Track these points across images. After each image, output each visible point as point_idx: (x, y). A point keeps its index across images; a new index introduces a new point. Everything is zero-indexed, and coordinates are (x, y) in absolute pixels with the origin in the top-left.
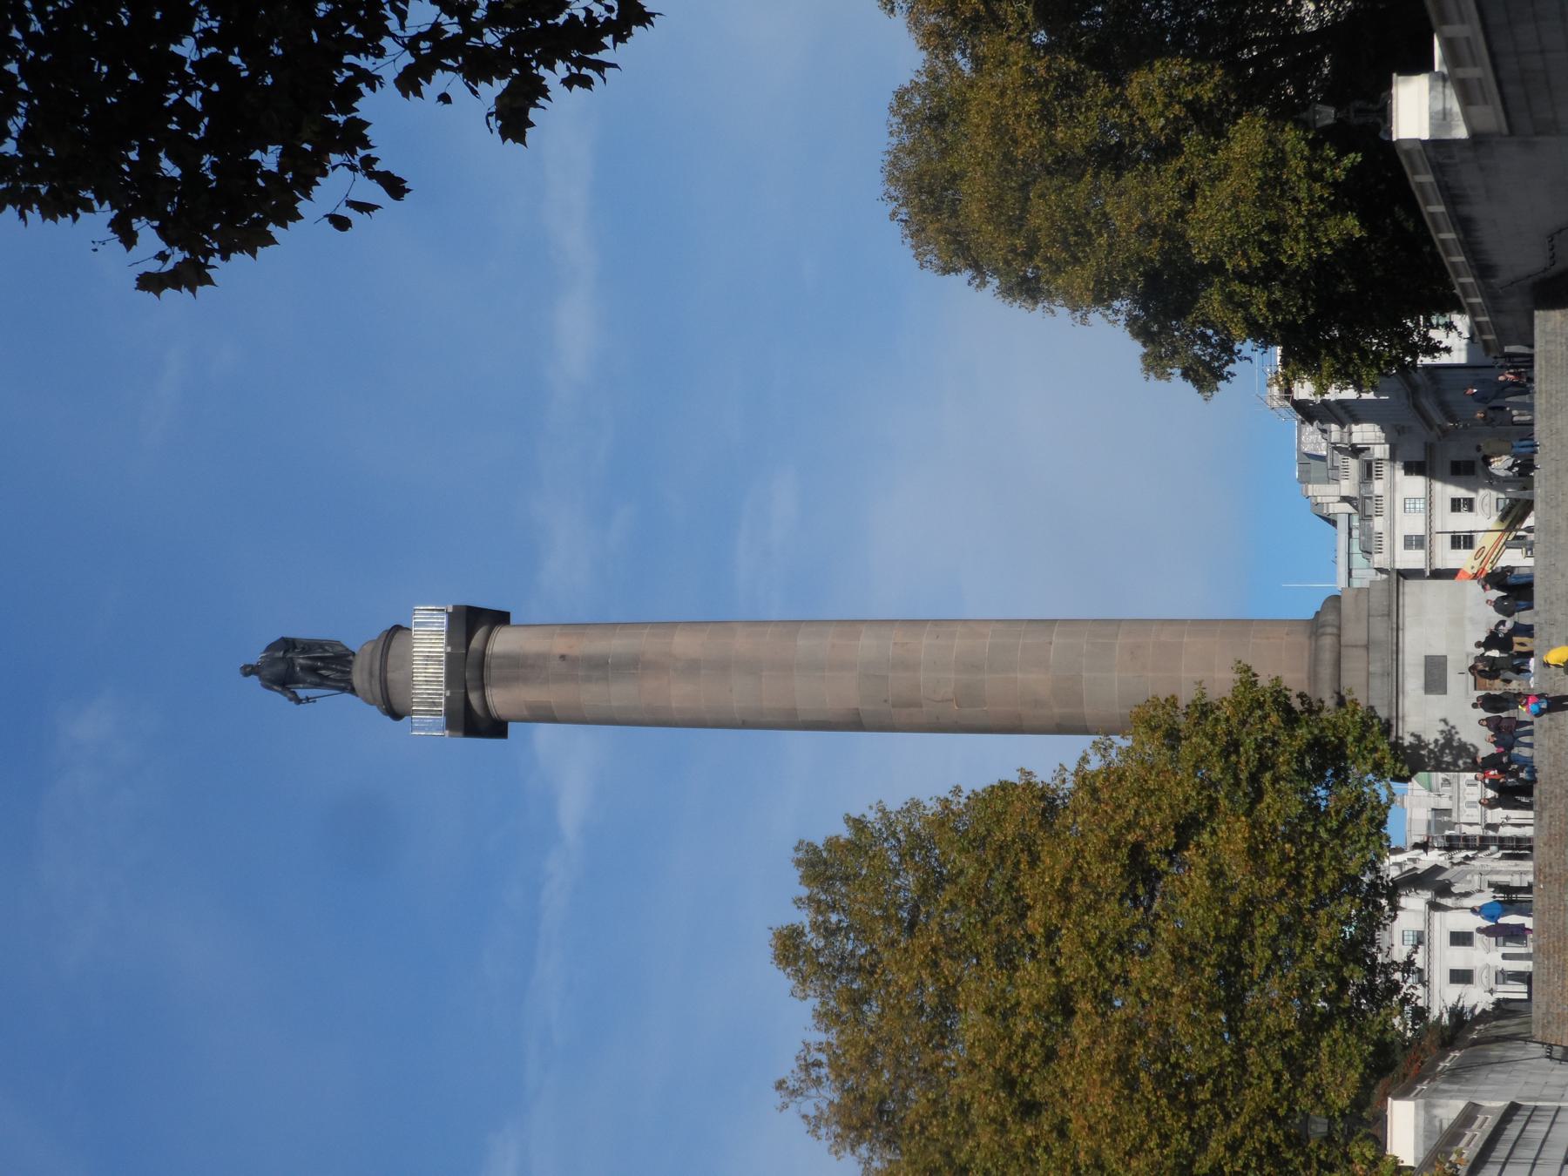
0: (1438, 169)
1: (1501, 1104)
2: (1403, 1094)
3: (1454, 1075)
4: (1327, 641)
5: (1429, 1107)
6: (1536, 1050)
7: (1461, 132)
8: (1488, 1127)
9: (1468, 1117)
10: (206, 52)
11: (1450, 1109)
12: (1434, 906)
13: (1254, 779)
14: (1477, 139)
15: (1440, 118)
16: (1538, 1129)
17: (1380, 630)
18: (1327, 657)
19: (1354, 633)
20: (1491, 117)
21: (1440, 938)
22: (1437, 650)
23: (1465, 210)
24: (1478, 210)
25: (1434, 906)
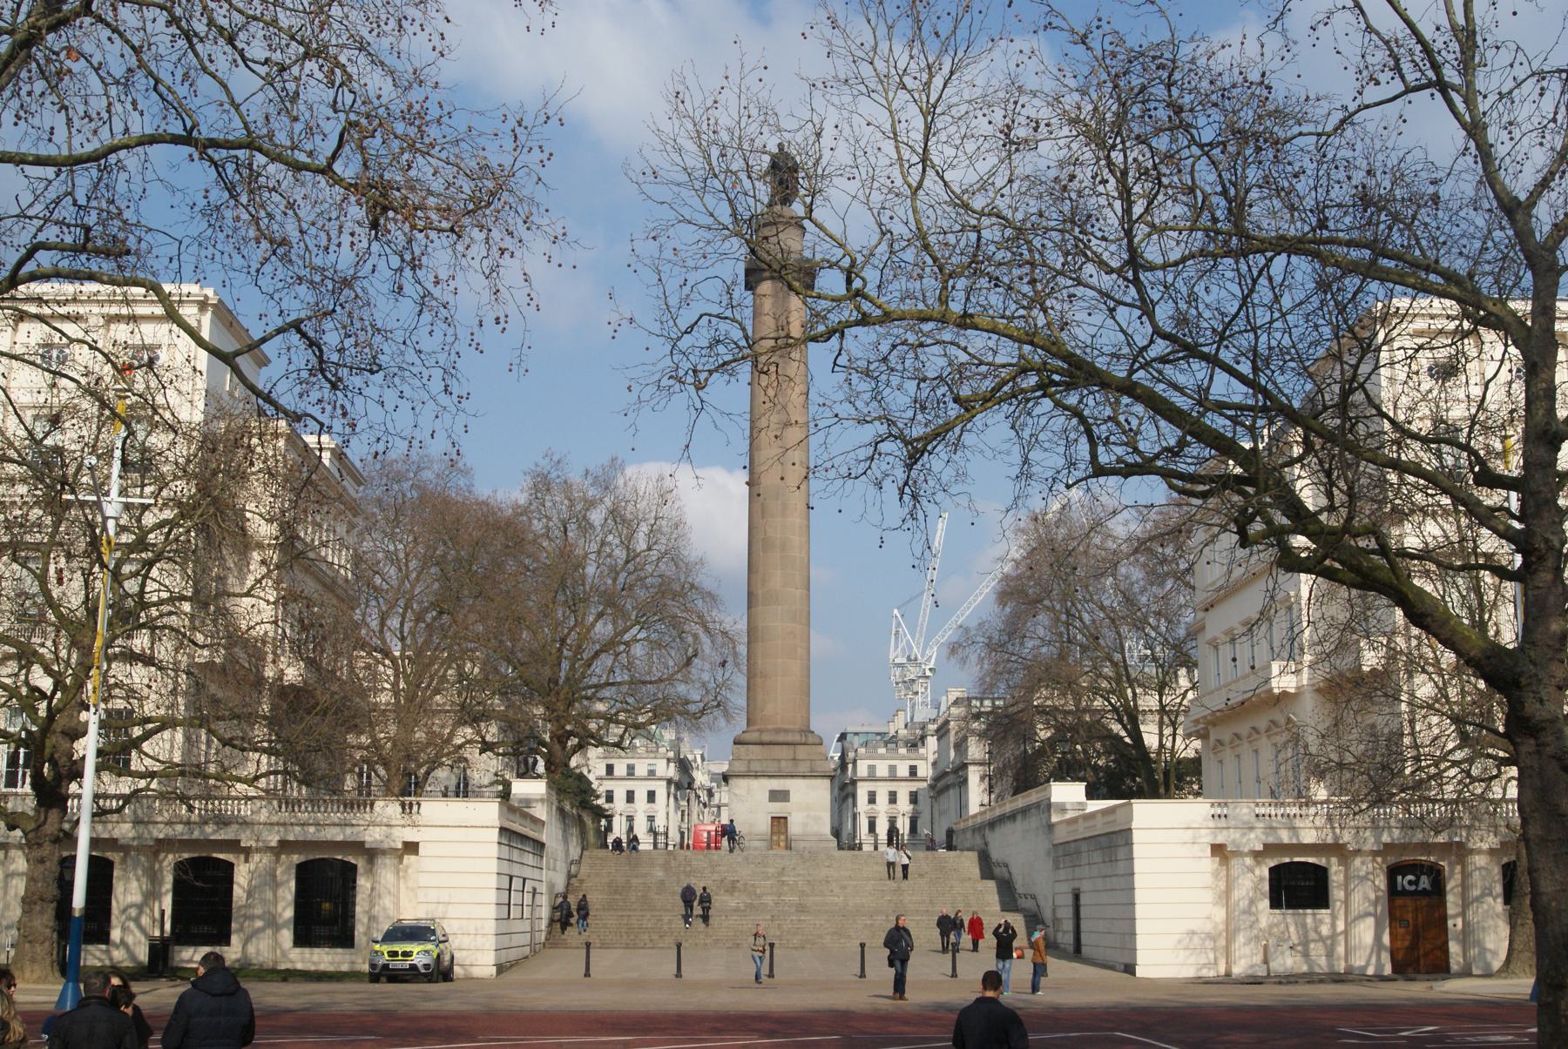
0: (1037, 805)
1: (544, 838)
2: (549, 786)
3: (561, 810)
4: (797, 738)
5: (542, 800)
6: (575, 852)
7: (1055, 819)
8: (531, 834)
9: (535, 821)
10: (541, 767)
11: (540, 812)
12: (669, 781)
13: (1397, 60)
14: (1051, 827)
15: (1062, 808)
16: (530, 859)
17: (803, 768)
18: (789, 738)
19: (802, 752)
20: (1061, 835)
21: (651, 785)
22: (792, 796)
23: (1019, 817)
24: (1019, 825)
25: (669, 781)
